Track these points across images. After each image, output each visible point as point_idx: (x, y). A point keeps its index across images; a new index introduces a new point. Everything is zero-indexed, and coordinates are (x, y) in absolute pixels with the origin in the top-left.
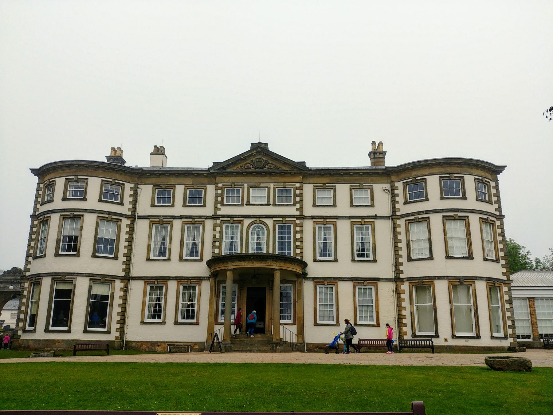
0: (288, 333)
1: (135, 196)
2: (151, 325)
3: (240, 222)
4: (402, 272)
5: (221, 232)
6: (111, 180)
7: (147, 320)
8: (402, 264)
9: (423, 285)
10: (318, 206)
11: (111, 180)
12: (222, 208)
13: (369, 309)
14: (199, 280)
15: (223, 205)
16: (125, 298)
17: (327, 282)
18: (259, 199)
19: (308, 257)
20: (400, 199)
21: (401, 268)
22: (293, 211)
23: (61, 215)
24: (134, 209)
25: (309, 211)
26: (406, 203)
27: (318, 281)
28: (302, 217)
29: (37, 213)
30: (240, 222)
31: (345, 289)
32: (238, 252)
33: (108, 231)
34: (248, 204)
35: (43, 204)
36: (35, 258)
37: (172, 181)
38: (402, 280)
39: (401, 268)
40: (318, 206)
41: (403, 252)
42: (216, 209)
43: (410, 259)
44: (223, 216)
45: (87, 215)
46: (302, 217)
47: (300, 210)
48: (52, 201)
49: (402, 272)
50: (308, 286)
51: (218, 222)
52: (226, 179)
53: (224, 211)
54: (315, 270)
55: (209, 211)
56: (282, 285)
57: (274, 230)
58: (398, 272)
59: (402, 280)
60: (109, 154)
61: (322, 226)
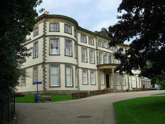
0: (119, 88)
2: (65, 82)
3: (102, 53)
4: (46, 60)
6: (53, 22)
8: (46, 57)
11: (53, 22)
12: (99, 47)
14: (95, 70)
20: (48, 28)
21: (46, 58)
26: (50, 31)
30: (102, 53)
32: (108, 63)
33: (53, 42)
37: (86, 34)
38: (46, 63)
39: (46, 58)
41: (47, 52)
43: (50, 55)
45: (61, 38)
49: (46, 60)
51: (98, 51)
52: (99, 38)
58: (45, 60)
59: (46, 63)
61: (83, 49)
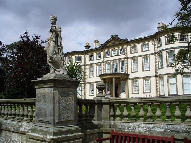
1: (85, 59)
5: (105, 67)
7: (91, 95)
9: (161, 77)
10: (144, 51)
13: (148, 87)
15: (105, 58)
16: (85, 88)
17: (135, 80)
18: (115, 54)
19: (129, 73)
22: (124, 56)
23: (166, 51)
24: (85, 63)
25: (129, 55)
27: (132, 79)
28: (127, 58)
29: (156, 52)
31: (141, 81)
34: (112, 56)
35: (158, 47)
36: (159, 69)
40: (144, 51)
42: (104, 59)
44: (106, 61)
46: (127, 58)
47: (127, 55)
48: (161, 46)
50: (130, 81)
51: (104, 63)
53: (106, 59)
54: (132, 76)
55: (101, 61)
56: (6, 92)
57: (119, 64)
60: (85, 45)
